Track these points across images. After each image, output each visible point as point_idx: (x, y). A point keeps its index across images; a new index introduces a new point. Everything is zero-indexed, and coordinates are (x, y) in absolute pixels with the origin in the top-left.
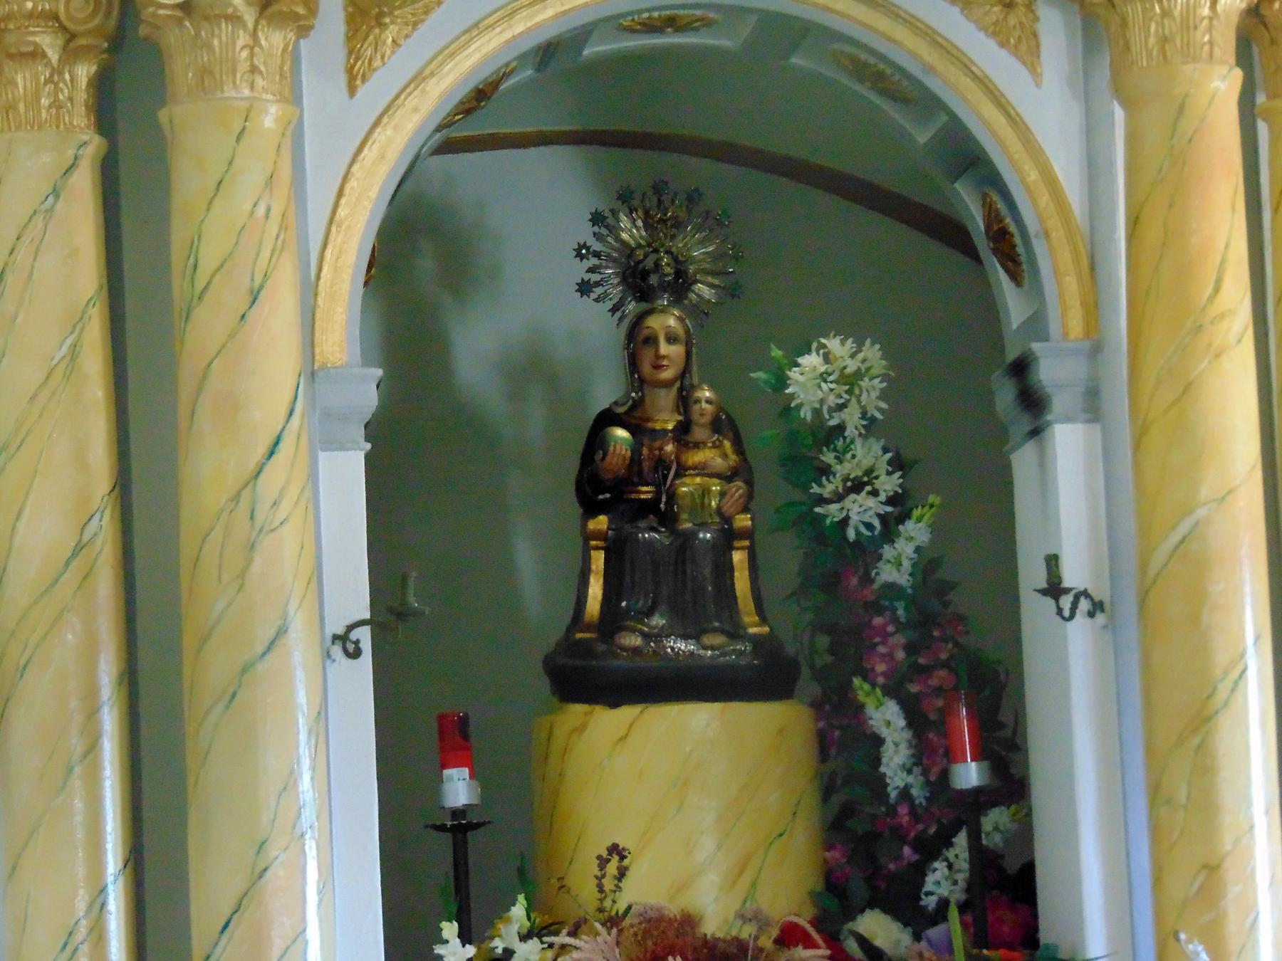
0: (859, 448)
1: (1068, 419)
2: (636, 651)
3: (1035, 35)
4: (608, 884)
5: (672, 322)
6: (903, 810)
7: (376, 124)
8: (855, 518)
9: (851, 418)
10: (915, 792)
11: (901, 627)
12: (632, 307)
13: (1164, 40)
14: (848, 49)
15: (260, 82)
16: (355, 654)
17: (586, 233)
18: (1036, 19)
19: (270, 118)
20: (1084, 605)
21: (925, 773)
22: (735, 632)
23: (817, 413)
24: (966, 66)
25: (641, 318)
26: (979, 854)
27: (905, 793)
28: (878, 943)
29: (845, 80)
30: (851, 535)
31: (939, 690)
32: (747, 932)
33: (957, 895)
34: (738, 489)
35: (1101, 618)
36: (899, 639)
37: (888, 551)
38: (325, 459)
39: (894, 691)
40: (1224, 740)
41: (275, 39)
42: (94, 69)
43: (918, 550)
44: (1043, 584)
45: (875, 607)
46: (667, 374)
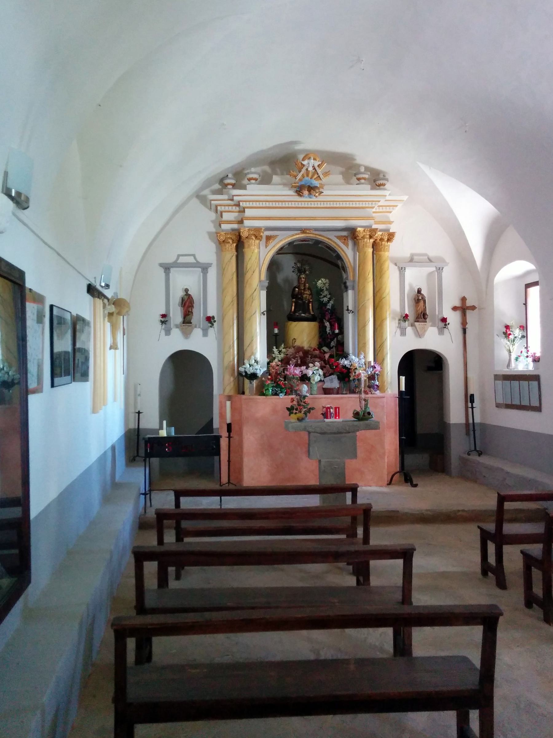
0: (325, 292)
1: (350, 290)
2: (298, 315)
3: (348, 244)
4: (293, 343)
5: (304, 276)
6: (329, 335)
7: (269, 252)
8: (324, 300)
9: (325, 288)
10: (330, 333)
11: (329, 314)
12: (299, 274)
13: (363, 245)
14: (325, 244)
15: (255, 246)
16: (264, 315)
17: (293, 265)
18: (348, 242)
19: (256, 251)
20: (351, 312)
21: (332, 331)
22: (310, 313)
23: (320, 288)
24: (340, 247)
25: (300, 275)
26: (337, 340)
27: (329, 333)
28: (325, 351)
29: (325, 248)
30: (324, 302)
31: (334, 321)
32: (310, 349)
33: (335, 345)
34: (311, 296)
35: (353, 313)
36: (329, 315)
37: (328, 304)
38: (261, 291)
39: (328, 321)
40: (367, 328)
41: (257, 241)
42: (236, 244)
43: (332, 304)
44: (346, 309)
45: (326, 311)
46: (303, 282)
